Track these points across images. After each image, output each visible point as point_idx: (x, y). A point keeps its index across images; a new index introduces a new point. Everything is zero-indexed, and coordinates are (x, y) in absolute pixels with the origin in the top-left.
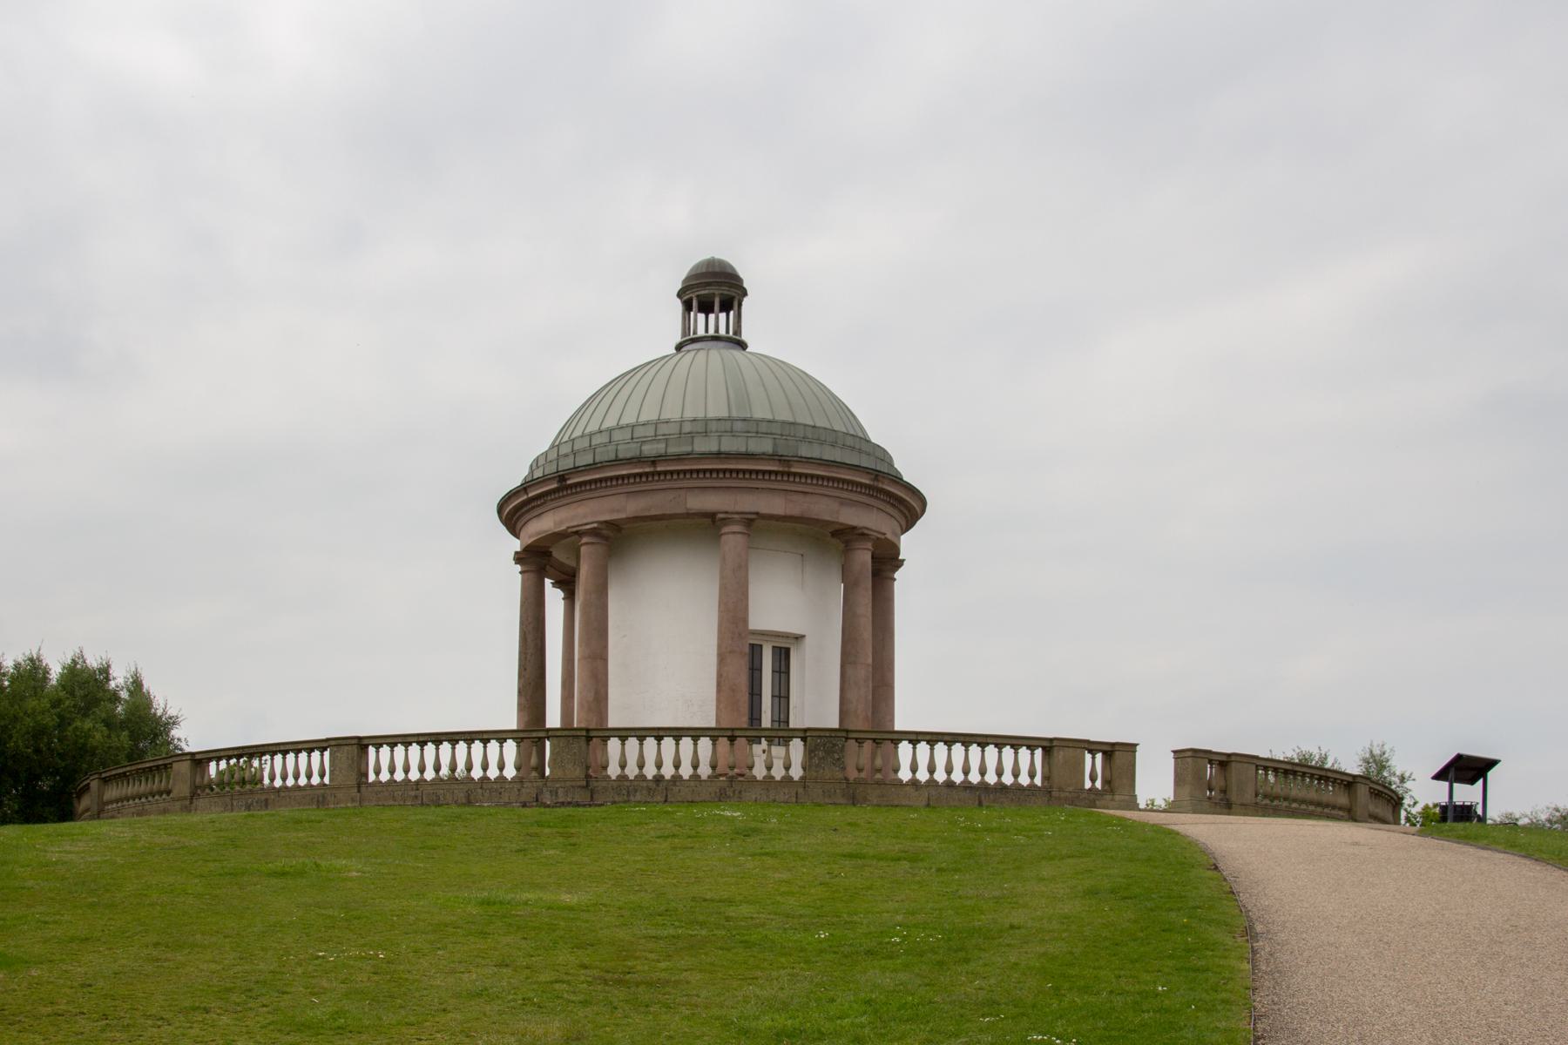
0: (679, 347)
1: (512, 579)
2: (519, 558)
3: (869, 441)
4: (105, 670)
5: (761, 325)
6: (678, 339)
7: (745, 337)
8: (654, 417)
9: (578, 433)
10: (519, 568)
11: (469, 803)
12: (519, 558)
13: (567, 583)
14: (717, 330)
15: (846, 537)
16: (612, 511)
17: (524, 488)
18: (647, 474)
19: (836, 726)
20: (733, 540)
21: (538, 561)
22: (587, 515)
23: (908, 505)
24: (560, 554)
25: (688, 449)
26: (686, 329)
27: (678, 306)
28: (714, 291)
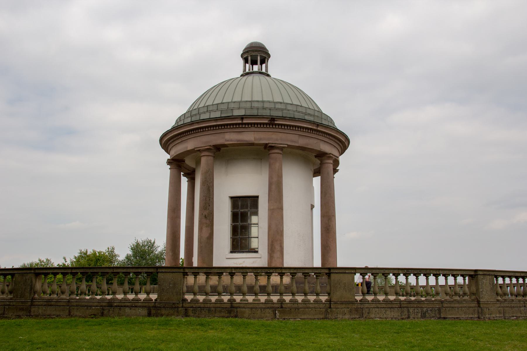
0: (242, 76)
1: (166, 171)
2: (169, 162)
3: (322, 113)
4: (111, 252)
5: (275, 67)
6: (242, 73)
7: (269, 73)
8: (239, 100)
9: (202, 105)
10: (169, 167)
11: (102, 315)
12: (169, 162)
13: (191, 176)
14: (249, 70)
15: (321, 155)
16: (292, 141)
17: (174, 129)
18: (239, 124)
19: (320, 266)
20: (275, 155)
21: (177, 164)
22: (200, 143)
23: (342, 142)
24: (189, 162)
25: (231, 115)
26: (245, 70)
27: (241, 61)
28: (256, 55)
